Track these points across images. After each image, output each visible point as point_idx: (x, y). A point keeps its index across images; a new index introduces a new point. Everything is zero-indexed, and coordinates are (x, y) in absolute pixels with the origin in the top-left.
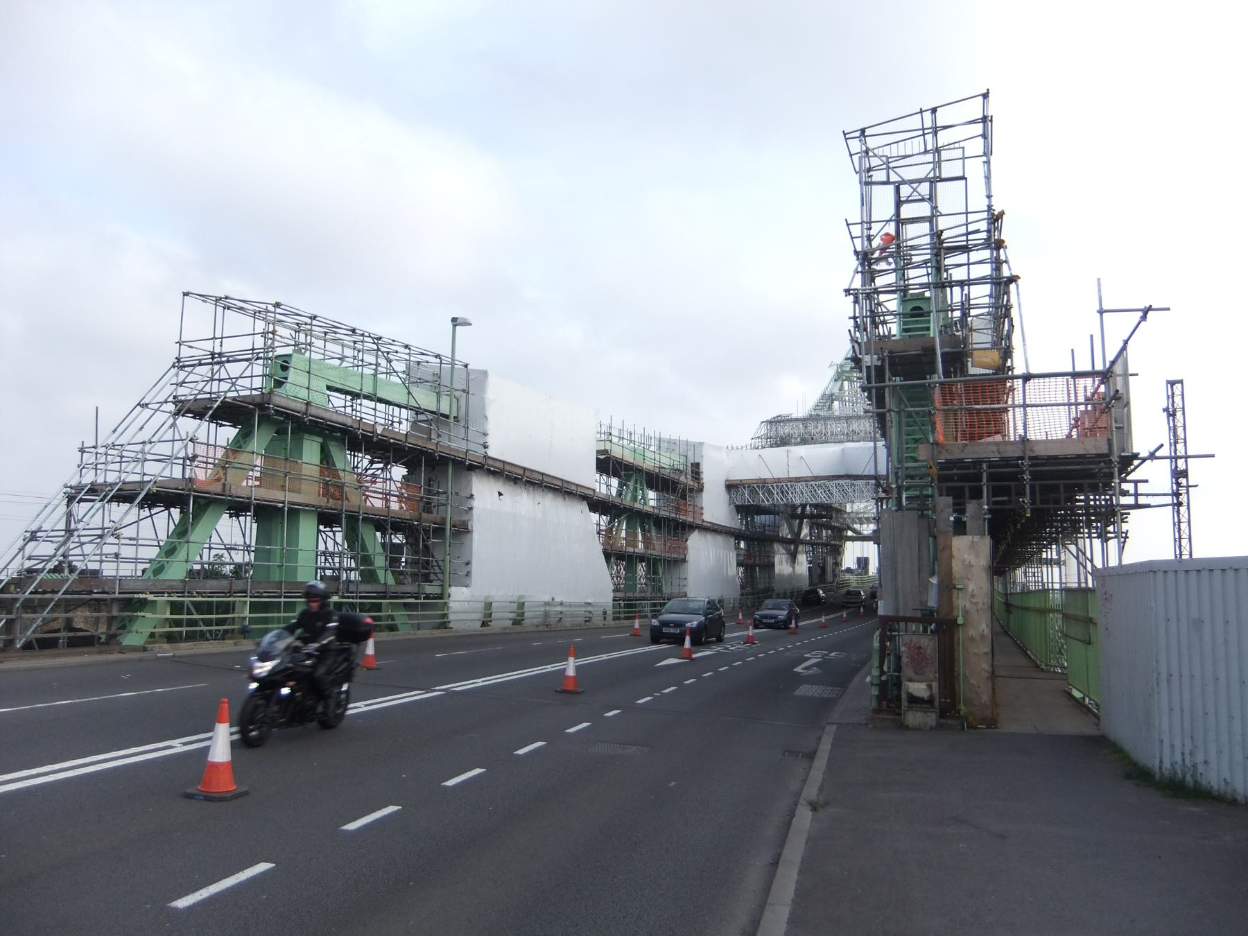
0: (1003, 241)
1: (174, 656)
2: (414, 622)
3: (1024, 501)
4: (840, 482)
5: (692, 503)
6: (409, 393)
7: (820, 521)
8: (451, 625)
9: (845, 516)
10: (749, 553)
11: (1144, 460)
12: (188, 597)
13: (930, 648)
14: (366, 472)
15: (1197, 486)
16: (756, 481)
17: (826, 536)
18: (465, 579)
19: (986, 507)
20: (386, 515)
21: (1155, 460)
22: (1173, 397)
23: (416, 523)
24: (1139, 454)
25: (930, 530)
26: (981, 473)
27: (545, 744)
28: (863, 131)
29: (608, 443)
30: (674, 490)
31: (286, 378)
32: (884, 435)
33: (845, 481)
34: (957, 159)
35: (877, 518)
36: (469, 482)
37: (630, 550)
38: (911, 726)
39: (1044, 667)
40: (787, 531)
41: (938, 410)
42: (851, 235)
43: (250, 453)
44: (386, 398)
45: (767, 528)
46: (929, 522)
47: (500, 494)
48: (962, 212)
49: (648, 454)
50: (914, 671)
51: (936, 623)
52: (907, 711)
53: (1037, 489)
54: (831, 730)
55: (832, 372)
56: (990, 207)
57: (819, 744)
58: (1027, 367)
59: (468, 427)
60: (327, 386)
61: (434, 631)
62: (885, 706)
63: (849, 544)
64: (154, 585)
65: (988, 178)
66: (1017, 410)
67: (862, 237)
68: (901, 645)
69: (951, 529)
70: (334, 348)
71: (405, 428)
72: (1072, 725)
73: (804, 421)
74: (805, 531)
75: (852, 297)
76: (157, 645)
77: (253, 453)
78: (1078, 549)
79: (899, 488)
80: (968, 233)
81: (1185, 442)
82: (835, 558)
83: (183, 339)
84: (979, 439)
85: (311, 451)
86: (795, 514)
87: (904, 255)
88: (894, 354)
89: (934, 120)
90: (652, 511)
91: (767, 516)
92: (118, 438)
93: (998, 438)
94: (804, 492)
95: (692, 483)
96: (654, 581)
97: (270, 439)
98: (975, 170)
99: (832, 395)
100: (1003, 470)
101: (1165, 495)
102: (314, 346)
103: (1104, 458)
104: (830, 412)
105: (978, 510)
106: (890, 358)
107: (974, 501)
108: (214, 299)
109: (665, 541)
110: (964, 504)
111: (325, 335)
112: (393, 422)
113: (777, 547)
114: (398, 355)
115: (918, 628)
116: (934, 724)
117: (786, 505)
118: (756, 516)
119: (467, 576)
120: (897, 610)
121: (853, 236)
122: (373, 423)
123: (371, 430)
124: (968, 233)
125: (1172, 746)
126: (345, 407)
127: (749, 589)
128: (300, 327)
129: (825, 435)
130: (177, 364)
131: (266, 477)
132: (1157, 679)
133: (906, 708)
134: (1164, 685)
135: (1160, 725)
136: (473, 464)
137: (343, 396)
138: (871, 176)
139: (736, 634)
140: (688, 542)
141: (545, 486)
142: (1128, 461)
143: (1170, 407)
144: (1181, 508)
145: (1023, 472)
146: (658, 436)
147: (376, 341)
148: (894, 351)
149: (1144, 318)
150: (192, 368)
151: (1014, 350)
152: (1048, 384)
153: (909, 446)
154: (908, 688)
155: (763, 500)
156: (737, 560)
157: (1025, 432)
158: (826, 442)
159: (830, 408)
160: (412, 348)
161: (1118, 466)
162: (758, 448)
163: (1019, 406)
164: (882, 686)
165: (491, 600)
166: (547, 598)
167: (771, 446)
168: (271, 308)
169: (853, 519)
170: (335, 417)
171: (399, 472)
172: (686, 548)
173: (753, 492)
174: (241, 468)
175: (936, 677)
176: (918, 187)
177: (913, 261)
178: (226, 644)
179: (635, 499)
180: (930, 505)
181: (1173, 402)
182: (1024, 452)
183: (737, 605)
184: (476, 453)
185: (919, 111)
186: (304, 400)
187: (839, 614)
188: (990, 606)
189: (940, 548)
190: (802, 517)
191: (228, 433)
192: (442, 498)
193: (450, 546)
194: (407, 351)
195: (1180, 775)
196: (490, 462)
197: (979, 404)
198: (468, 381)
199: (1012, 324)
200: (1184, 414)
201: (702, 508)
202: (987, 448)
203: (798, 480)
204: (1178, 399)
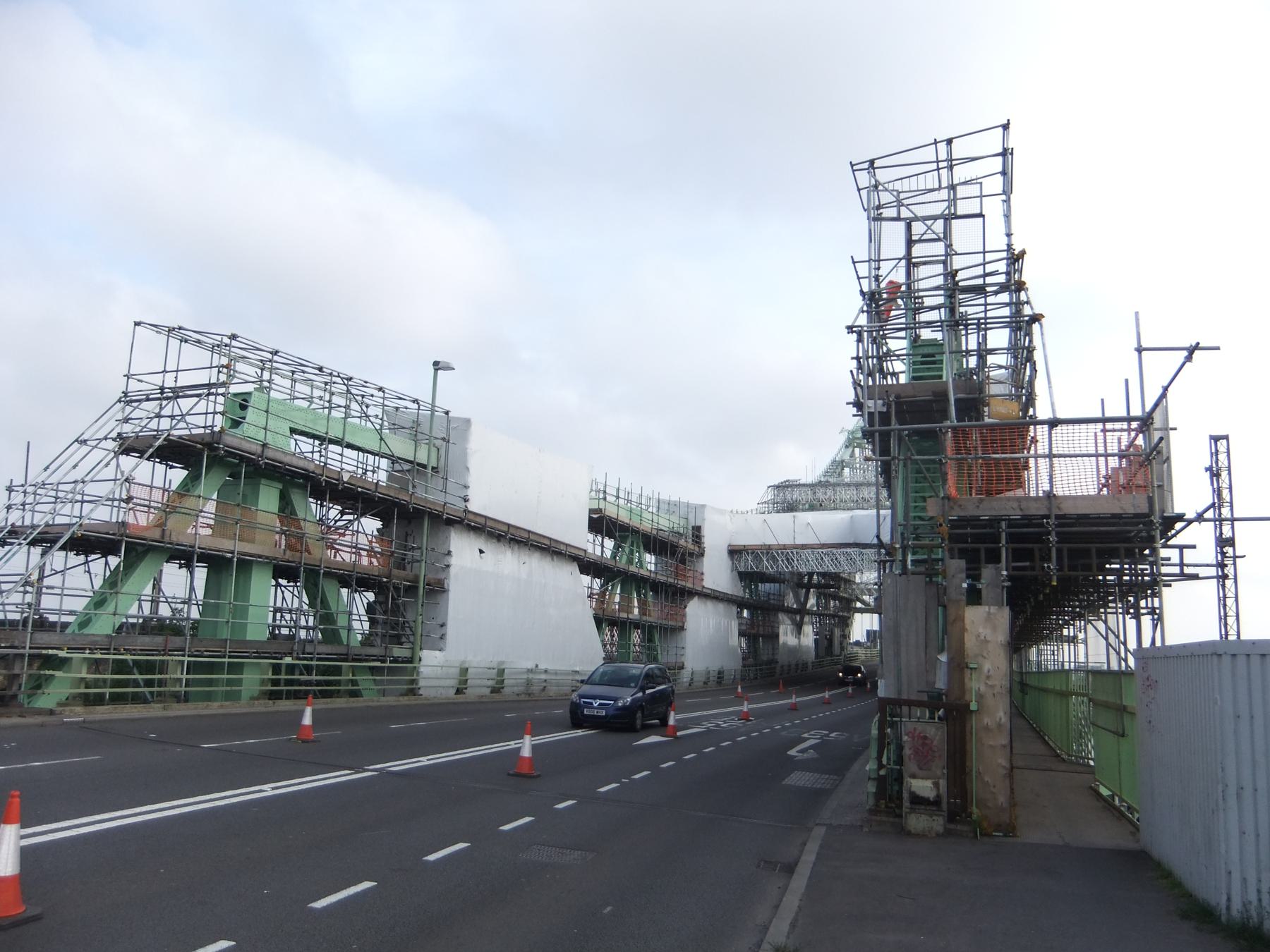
0: (1024, 283)
1: (84, 721)
2: (380, 687)
3: (1049, 567)
4: (848, 550)
5: (692, 568)
6: (381, 439)
7: (827, 591)
8: (421, 692)
9: (854, 587)
10: (752, 622)
11: (1190, 522)
12: (114, 654)
13: (937, 738)
14: (335, 523)
15: (1245, 556)
16: (760, 547)
17: (834, 606)
18: (439, 642)
19: (1005, 573)
20: (351, 569)
21: (1203, 523)
22: (1217, 455)
23: (385, 580)
24: (1184, 515)
25: (940, 599)
26: (1000, 534)
27: (468, 847)
28: (872, 162)
29: (602, 502)
30: (673, 554)
31: (244, 418)
32: (888, 484)
33: (853, 549)
34: (974, 197)
35: (879, 584)
36: (447, 537)
37: (624, 615)
38: (913, 831)
39: (1065, 757)
40: (793, 600)
41: (951, 459)
42: (858, 275)
43: (196, 497)
44: (357, 444)
45: (772, 597)
46: (938, 589)
47: (481, 552)
48: (979, 251)
49: (645, 515)
50: (918, 765)
51: (945, 709)
52: (910, 813)
53: (1065, 553)
54: (820, 832)
55: (843, 438)
56: (1009, 246)
57: (801, 852)
58: (1054, 411)
59: (446, 479)
60: (290, 428)
61: (401, 698)
62: (883, 806)
63: (857, 616)
64: (74, 640)
65: (1007, 216)
66: (1041, 460)
67: (869, 277)
68: (903, 733)
69: (964, 598)
70: (302, 389)
71: (382, 476)
72: (1105, 835)
73: (812, 486)
74: (812, 601)
75: (855, 335)
76: (67, 709)
77: (199, 497)
78: (1108, 628)
79: (905, 548)
80: (985, 275)
81: (1231, 506)
82: (843, 631)
83: (131, 373)
84: (996, 494)
85: (268, 498)
86: (801, 583)
87: (915, 298)
88: (902, 400)
89: (950, 152)
90: (649, 575)
91: (772, 584)
92: (49, 476)
93: (1019, 493)
94: (810, 560)
95: (692, 547)
96: (649, 649)
97: (221, 484)
98: (993, 208)
99: (843, 461)
100: (1025, 530)
101: (1208, 565)
102: (274, 384)
103: (1143, 519)
104: (840, 479)
105: (994, 576)
106: (896, 403)
107: (990, 566)
108: (167, 329)
109: (662, 607)
110: (979, 569)
111: (293, 374)
112: (366, 470)
113: (782, 617)
114: (374, 398)
115: (923, 716)
116: (941, 829)
117: (792, 573)
118: (760, 584)
119: (441, 638)
120: (899, 692)
121: (860, 276)
122: (339, 470)
123: (336, 477)
124: (985, 275)
125: (1244, 880)
126: (312, 452)
127: (751, 661)
128: (264, 364)
129: (834, 501)
130: (123, 399)
131: (220, 525)
132: (1223, 791)
133: (908, 810)
134: (1232, 801)
135: (1226, 852)
136: (452, 519)
137: (311, 441)
138: (881, 213)
139: (731, 709)
140: (687, 609)
141: (532, 545)
142: (1170, 522)
143: (1214, 465)
144: (1226, 581)
145: (1049, 533)
146: (656, 496)
147: (346, 382)
148: (902, 395)
149: (1189, 358)
150: (138, 403)
151: (1037, 398)
152: (1078, 431)
153: (917, 504)
154: (911, 786)
155: (767, 567)
156: (739, 630)
157: (1051, 486)
158: (835, 509)
159: (840, 475)
160: (386, 391)
161: (1160, 528)
162: (764, 513)
163: (1044, 456)
164: (881, 781)
165: (467, 666)
166: (530, 665)
167: (778, 512)
168: (226, 340)
169: (862, 590)
170: (295, 461)
171: (371, 525)
172: (684, 615)
173: (757, 557)
174: (186, 514)
175: (944, 773)
176: (933, 224)
177: (925, 305)
178: (154, 708)
179: (630, 561)
180: (940, 570)
181: (1217, 459)
182: (1050, 509)
183: (738, 677)
184: (455, 507)
185: (933, 141)
186: (261, 441)
187: (844, 689)
188: (1009, 690)
189: (951, 618)
190: (809, 586)
191: (178, 475)
192: (417, 554)
193: (422, 605)
194: (381, 394)
195: (1254, 913)
196: (471, 517)
197: (998, 453)
198: (448, 429)
199: (1035, 368)
200: (1230, 474)
201: (702, 574)
202: (1005, 505)
203: (804, 547)
204: (1222, 458)
